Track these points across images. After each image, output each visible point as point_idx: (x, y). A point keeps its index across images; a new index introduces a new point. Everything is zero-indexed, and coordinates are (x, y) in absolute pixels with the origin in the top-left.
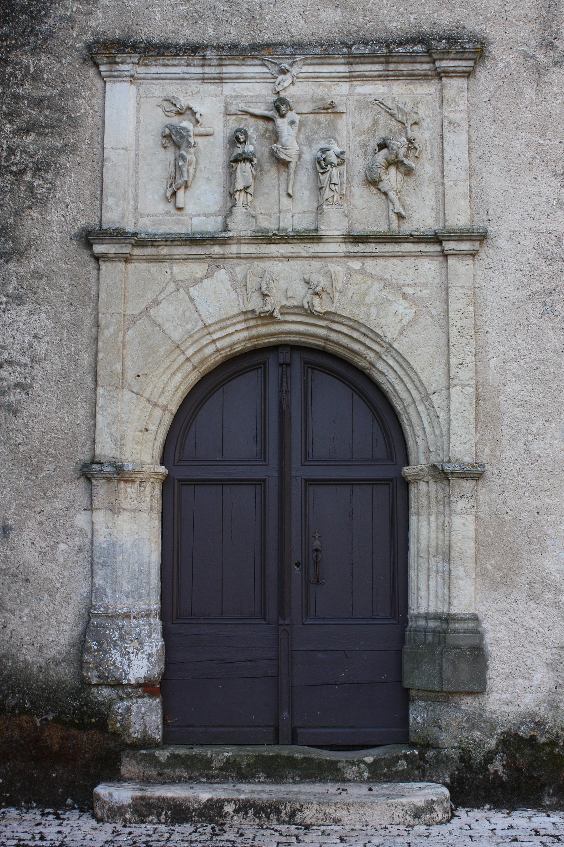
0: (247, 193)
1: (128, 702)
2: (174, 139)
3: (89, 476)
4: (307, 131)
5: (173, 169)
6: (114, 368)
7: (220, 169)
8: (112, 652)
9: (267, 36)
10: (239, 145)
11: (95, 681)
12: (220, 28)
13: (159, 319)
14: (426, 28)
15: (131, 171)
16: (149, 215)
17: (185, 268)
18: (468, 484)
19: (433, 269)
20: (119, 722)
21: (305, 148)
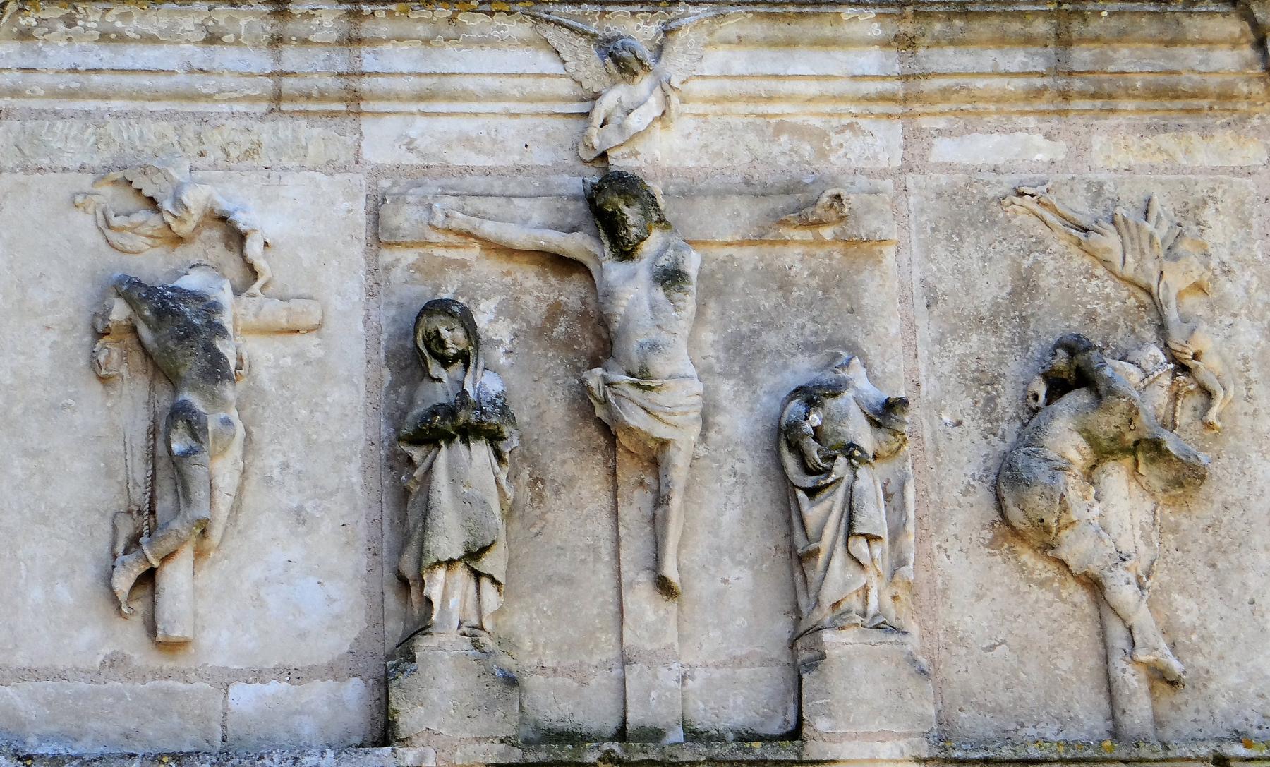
0: (478, 575)
2: (166, 341)
4: (734, 315)
7: (353, 474)
10: (435, 368)
16: (31, 673)
21: (726, 388)
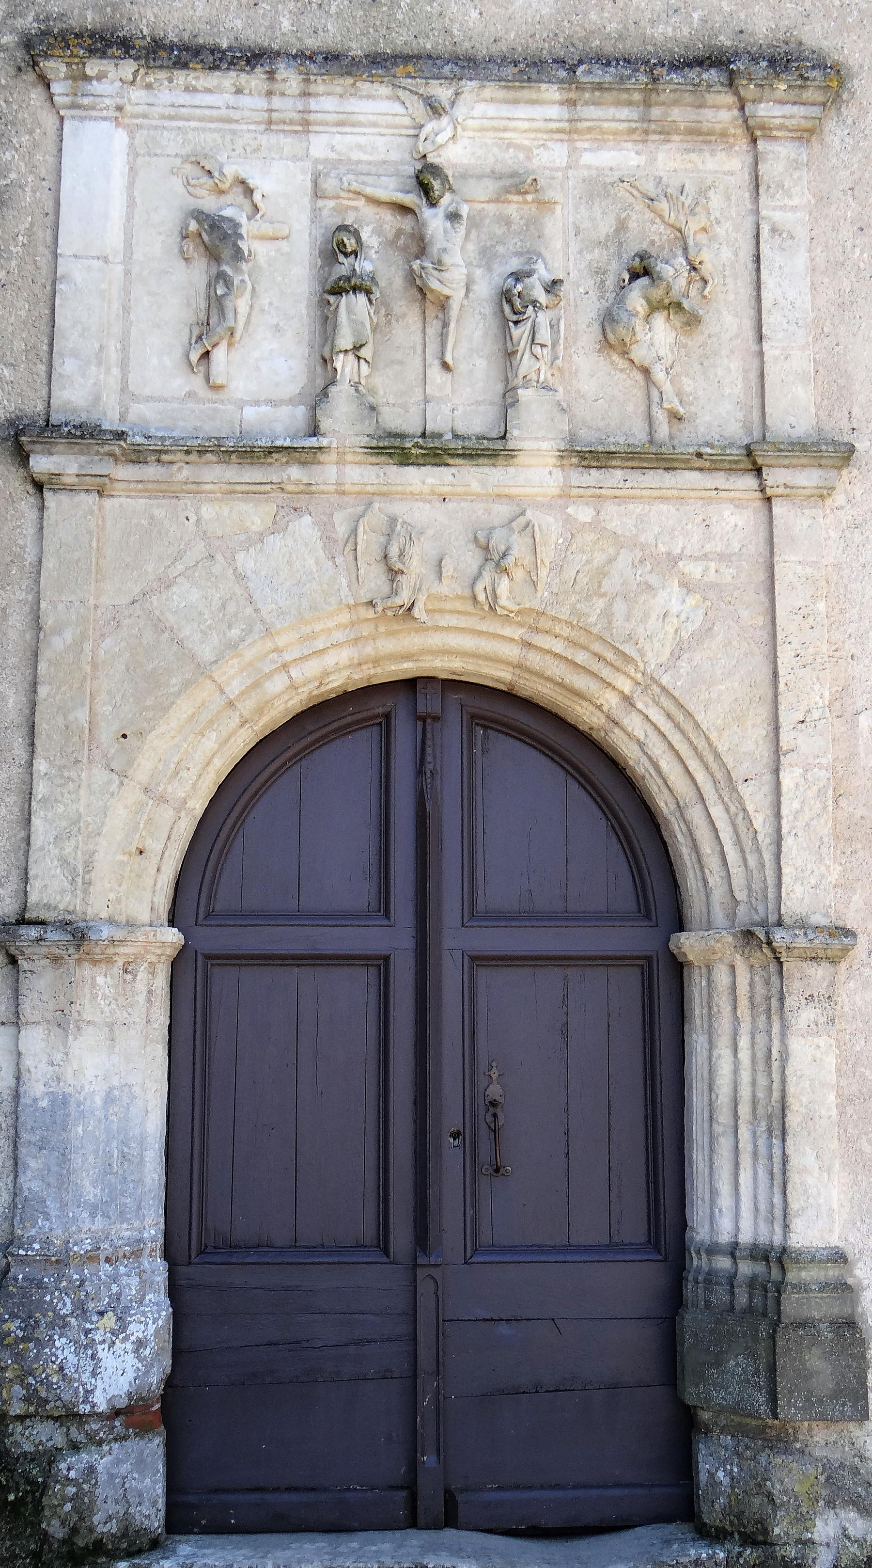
0: (359, 358)
1: (89, 1453)
3: (12, 950)
4: (483, 236)
5: (203, 305)
6: (71, 718)
8: (57, 1344)
9: (401, 40)
10: (341, 258)
11: (17, 1409)
12: (306, 20)
13: (170, 616)
14: (725, 40)
15: (116, 306)
17: (226, 510)
18: (820, 972)
19: (740, 524)
20: (72, 1499)
21: (478, 272)
